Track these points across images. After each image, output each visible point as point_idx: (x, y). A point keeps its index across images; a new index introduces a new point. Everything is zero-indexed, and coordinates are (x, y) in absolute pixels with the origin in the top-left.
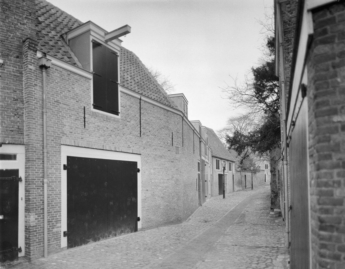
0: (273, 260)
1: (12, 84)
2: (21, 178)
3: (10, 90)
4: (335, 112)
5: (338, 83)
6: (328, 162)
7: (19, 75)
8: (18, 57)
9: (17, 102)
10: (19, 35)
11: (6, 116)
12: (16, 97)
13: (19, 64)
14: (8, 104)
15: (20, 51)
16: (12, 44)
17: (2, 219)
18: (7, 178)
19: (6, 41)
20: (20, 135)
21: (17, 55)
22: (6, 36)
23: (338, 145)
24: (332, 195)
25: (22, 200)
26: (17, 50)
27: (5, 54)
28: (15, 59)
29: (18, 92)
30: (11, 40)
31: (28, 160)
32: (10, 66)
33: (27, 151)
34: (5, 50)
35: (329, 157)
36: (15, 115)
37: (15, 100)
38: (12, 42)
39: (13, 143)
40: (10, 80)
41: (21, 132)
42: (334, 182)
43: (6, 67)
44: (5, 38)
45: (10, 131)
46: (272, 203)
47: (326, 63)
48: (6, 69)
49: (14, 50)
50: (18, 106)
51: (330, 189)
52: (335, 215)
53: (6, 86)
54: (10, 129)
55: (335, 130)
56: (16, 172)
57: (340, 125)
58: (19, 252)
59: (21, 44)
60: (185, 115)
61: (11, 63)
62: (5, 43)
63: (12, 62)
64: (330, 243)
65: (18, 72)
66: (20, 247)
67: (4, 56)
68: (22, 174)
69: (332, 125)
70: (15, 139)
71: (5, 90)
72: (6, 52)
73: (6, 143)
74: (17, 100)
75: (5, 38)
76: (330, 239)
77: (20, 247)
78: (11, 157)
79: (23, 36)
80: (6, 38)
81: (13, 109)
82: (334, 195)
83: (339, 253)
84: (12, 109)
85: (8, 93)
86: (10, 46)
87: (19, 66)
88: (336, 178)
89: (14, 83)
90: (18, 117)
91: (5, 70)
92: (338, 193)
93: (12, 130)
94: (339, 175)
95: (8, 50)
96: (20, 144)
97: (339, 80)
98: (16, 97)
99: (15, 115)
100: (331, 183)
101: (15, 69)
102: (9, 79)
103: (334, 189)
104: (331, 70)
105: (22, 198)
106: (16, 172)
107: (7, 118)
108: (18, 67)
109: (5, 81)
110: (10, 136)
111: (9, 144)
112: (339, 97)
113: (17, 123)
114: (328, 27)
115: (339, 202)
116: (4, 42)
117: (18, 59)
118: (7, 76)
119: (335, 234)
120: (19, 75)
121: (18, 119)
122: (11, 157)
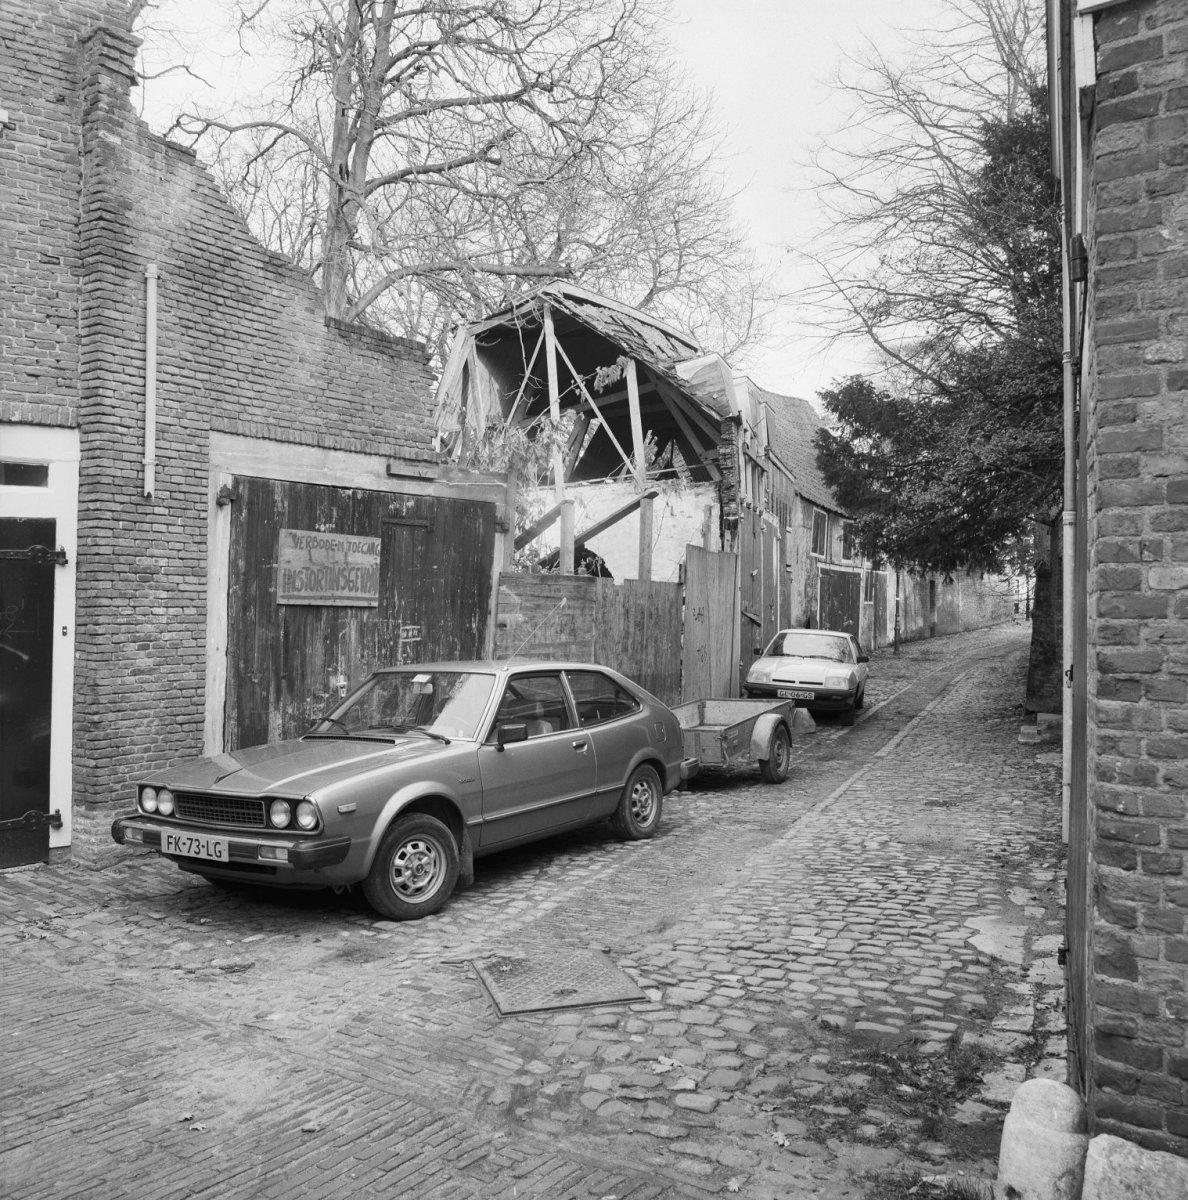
0: (586, 1085)
1: (40, 199)
2: (63, 554)
3: (31, 223)
4: (1152, 332)
5: (1164, 242)
6: (1125, 487)
7: (63, 165)
8: (61, 100)
9: (57, 267)
10: (68, 14)
11: (14, 321)
12: (50, 251)
13: (65, 125)
14: (22, 275)
15: (69, 77)
16: (42, 51)
17: (649, 716)
18: (12, 551)
19: (19, 37)
20: (64, 390)
21: (59, 90)
22: (18, 19)
23: (1156, 431)
24: (1137, 587)
25: (65, 634)
26: (60, 74)
27: (15, 88)
28: (52, 106)
29: (59, 231)
30: (37, 34)
31: (89, 482)
32: (33, 132)
33: (89, 452)
34: (15, 71)
35: (1129, 469)
36: (48, 316)
37: (47, 259)
38: (40, 43)
39: (36, 421)
40: (31, 185)
41: (68, 382)
42: (1143, 546)
43: (19, 137)
44: (15, 27)
45: (29, 375)
46: (1032, 691)
47: (1130, 180)
48: (17, 144)
49: (49, 71)
50: (59, 282)
51: (1130, 566)
52: (1143, 648)
53: (19, 207)
54: (29, 369)
55: (1151, 389)
56: (44, 530)
57: (1163, 371)
58: (51, 829)
59: (74, 51)
60: (475, 102)
61: (36, 121)
62: (16, 45)
63: (40, 118)
64: (1127, 733)
65: (62, 156)
66: (58, 812)
67: (11, 95)
68: (66, 539)
69: (1143, 372)
70: (46, 406)
71: (11, 223)
72: (18, 80)
73: (13, 419)
74: (55, 260)
75: (15, 27)
76: (1126, 721)
77: (58, 812)
78: (31, 474)
79: (83, 19)
80: (20, 28)
81: (41, 295)
82: (1143, 586)
83: (1152, 762)
84: (35, 296)
85: (21, 233)
86: (35, 59)
87: (65, 132)
88: (1149, 535)
89: (44, 196)
90: (58, 326)
91: (13, 148)
92: (1154, 578)
93: (36, 373)
94: (1157, 524)
95: (26, 74)
96: (61, 426)
97: (1165, 233)
98: (50, 248)
99: (48, 316)
100: (1134, 549)
101: (49, 142)
102: (27, 183)
103: (1143, 568)
104: (1144, 201)
105: (65, 628)
106: (44, 530)
107: (19, 326)
108: (60, 135)
109: (13, 190)
110: (27, 396)
111: (21, 423)
112: (1163, 287)
113: (54, 348)
114: (1137, 68)
115: (1155, 609)
116: (13, 40)
117: (62, 108)
118: (23, 169)
119: (1143, 704)
120: (63, 165)
121: (59, 331)
122: (31, 474)
